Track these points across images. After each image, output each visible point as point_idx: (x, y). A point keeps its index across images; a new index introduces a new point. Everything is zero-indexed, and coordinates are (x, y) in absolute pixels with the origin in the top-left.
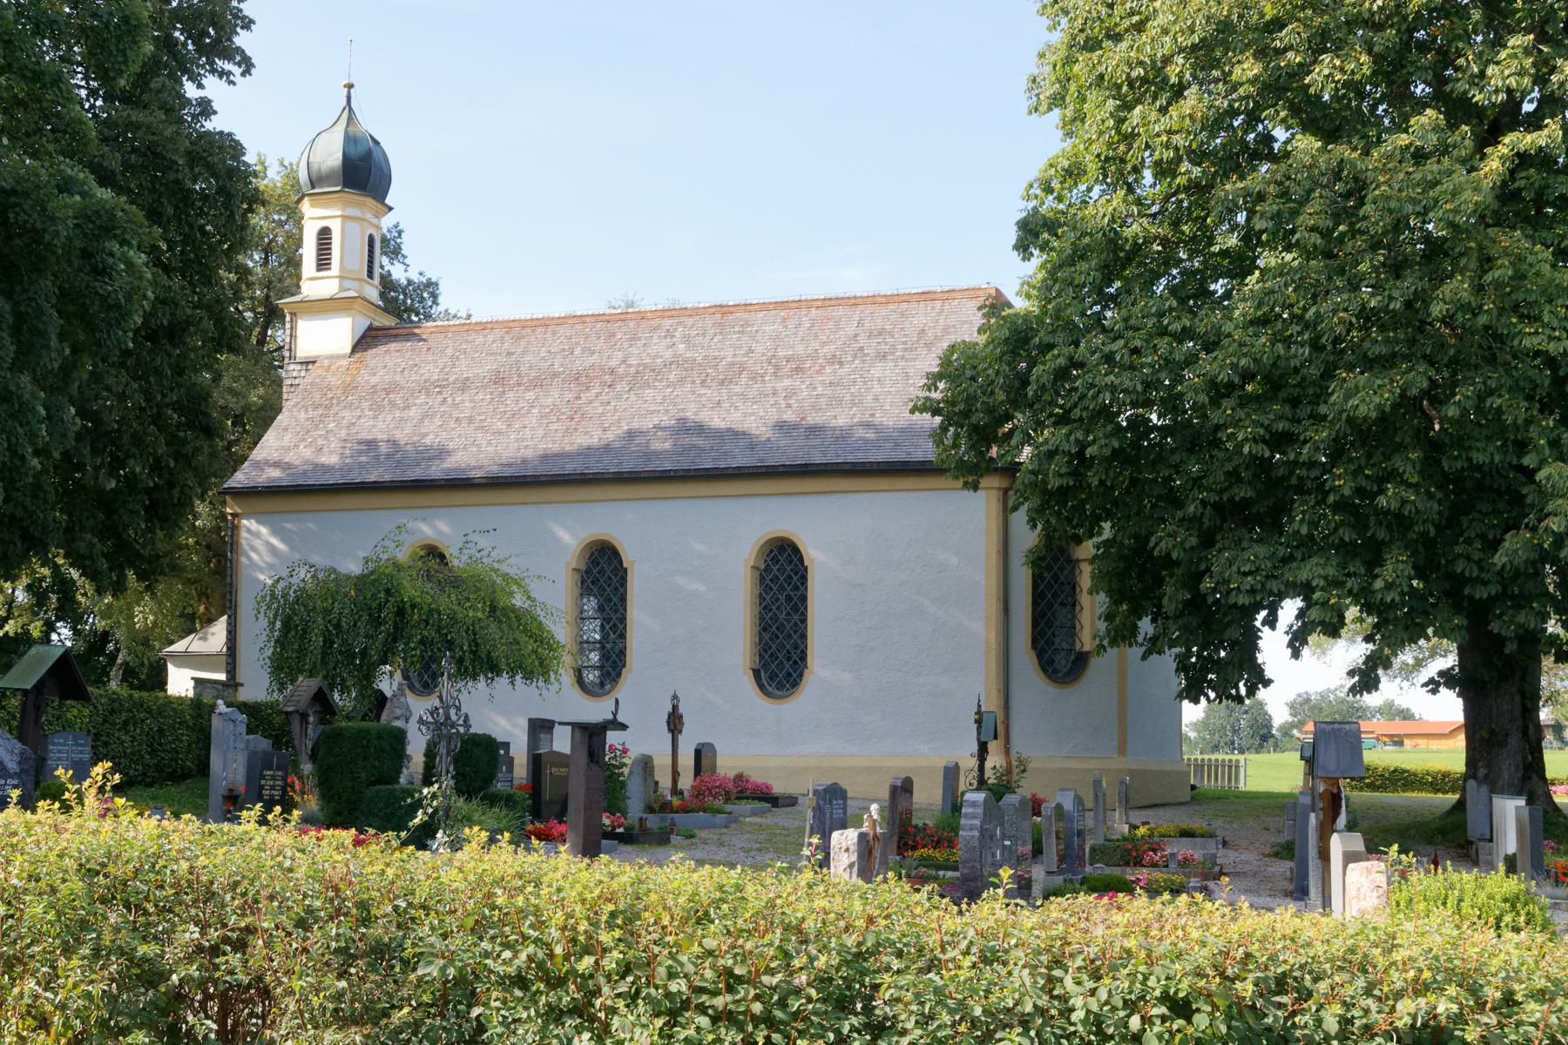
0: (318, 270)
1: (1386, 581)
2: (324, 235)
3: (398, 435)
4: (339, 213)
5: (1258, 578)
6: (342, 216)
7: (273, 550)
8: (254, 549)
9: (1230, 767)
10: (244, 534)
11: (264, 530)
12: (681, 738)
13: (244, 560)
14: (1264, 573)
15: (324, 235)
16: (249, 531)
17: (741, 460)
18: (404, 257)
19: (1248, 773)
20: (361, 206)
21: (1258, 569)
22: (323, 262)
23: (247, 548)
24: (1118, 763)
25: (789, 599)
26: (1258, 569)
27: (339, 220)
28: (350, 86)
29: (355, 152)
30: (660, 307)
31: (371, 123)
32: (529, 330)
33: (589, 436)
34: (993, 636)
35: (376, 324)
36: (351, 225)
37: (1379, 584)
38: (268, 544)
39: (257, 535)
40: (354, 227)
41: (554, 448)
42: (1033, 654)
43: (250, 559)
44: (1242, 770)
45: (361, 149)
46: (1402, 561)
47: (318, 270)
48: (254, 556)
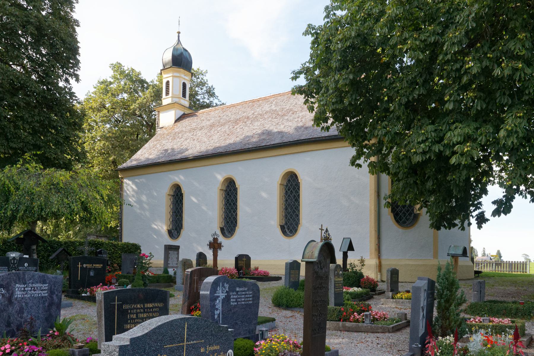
0: (166, 96)
1: (507, 130)
2: (168, 83)
3: (175, 147)
4: (171, 75)
5: (427, 144)
6: (172, 76)
7: (133, 190)
8: (128, 190)
9: (523, 264)
10: (124, 185)
11: (130, 183)
12: (219, 252)
13: (125, 194)
14: (430, 140)
15: (168, 83)
16: (126, 183)
17: (277, 141)
18: (218, 97)
19: (530, 267)
20: (179, 72)
21: (427, 139)
22: (167, 93)
23: (126, 189)
24: (435, 262)
25: (294, 196)
26: (427, 139)
27: (171, 77)
28: (179, 33)
29: (177, 53)
30: (272, 95)
31: (186, 44)
32: (229, 108)
33: (231, 140)
34: (373, 207)
35: (186, 113)
36: (175, 79)
37: (502, 133)
38: (132, 188)
39: (128, 185)
40: (177, 80)
41: (218, 145)
42: (392, 215)
43: (126, 193)
44: (528, 266)
45: (179, 52)
46: (520, 117)
47: (166, 96)
48: (128, 192)
